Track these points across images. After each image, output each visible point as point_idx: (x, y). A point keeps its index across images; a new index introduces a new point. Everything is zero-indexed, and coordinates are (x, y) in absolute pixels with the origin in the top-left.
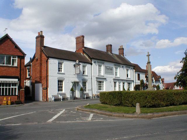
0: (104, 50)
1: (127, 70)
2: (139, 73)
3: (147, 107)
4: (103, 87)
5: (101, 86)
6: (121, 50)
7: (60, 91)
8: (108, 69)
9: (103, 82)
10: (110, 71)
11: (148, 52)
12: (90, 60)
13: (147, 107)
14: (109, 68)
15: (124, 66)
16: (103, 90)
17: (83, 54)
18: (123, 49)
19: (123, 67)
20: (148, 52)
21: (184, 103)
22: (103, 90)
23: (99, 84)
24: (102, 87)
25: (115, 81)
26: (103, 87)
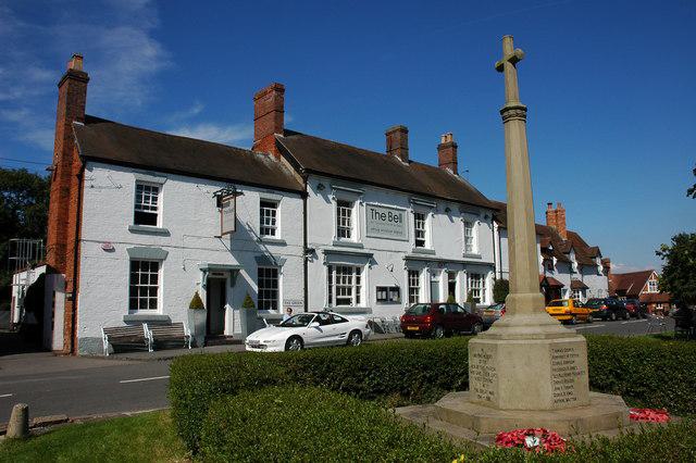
8: (382, 217)
14: (386, 211)
17: (278, 158)
24: (481, 292)
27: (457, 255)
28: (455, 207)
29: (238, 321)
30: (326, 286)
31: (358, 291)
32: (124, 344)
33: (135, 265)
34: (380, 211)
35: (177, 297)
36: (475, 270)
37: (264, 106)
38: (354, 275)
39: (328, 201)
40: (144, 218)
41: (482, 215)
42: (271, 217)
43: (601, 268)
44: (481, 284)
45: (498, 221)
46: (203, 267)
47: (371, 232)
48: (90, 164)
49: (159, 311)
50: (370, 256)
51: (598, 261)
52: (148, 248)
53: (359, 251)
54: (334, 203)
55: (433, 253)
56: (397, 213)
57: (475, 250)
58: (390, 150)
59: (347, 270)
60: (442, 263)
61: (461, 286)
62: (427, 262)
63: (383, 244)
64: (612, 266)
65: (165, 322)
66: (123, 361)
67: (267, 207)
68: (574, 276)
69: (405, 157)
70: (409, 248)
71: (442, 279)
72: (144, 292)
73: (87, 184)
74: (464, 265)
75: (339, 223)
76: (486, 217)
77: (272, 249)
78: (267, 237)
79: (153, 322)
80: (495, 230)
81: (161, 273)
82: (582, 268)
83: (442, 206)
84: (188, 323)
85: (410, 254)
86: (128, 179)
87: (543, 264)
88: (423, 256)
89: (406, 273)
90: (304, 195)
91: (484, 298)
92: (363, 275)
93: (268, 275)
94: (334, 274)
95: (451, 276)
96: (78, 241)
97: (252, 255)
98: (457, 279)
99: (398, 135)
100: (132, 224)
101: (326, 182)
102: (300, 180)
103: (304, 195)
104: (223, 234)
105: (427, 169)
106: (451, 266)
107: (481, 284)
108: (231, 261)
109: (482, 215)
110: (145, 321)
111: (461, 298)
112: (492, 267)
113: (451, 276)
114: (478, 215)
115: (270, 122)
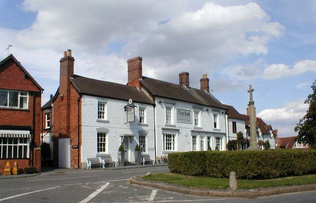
0: (176, 81)
1: (215, 116)
4: (174, 145)
5: (171, 143)
6: (205, 81)
7: (101, 151)
8: (182, 113)
14: (184, 111)
16: (174, 149)
17: (140, 89)
22: (174, 149)
24: (172, 144)
25: (195, 134)
26: (174, 145)
27: (211, 129)
28: (210, 109)
29: (133, 156)
30: (163, 143)
31: (174, 144)
32: (96, 166)
33: (99, 135)
34: (182, 111)
35: (112, 149)
36: (218, 136)
37: (133, 66)
38: (172, 138)
39: (163, 108)
40: (100, 114)
41: (221, 112)
42: (102, 107)
43: (272, 135)
44: (172, 140)
45: (227, 114)
46: (122, 135)
47: (179, 120)
48: (83, 96)
49: (107, 152)
50: (178, 130)
51: (271, 132)
52: (103, 128)
53: (201, 130)
54: (165, 108)
55: (220, 130)
56: (187, 112)
57: (199, 125)
58: (181, 83)
59: (170, 136)
60: (206, 133)
61: (213, 143)
62: (199, 132)
63: (183, 125)
64: (278, 133)
65: (109, 157)
66: (95, 171)
67: (142, 110)
68: (260, 139)
69: (188, 86)
70: (192, 127)
71: (205, 140)
72: (101, 144)
73: (82, 104)
74: (214, 133)
75: (99, 109)
76: (223, 113)
77: (144, 128)
78: (101, 119)
79: (103, 157)
80: (226, 118)
81: (107, 138)
82: (263, 134)
83: (205, 108)
84: (115, 159)
85: (193, 129)
86: (95, 101)
87: (247, 133)
88: (198, 130)
89: (192, 137)
90: (154, 106)
91: (174, 147)
92: (176, 138)
93: (142, 138)
94: (165, 137)
95: (209, 138)
96: (79, 126)
97: (137, 130)
98: (211, 140)
99: (185, 76)
100: (97, 119)
101: (162, 100)
102: (151, 99)
103: (154, 106)
104: (128, 122)
105: (197, 91)
106: (209, 134)
107: (172, 140)
108: (130, 133)
109: (221, 112)
110: (100, 156)
111: (213, 147)
112: (225, 134)
113: (209, 138)
114: (219, 112)
115: (136, 73)
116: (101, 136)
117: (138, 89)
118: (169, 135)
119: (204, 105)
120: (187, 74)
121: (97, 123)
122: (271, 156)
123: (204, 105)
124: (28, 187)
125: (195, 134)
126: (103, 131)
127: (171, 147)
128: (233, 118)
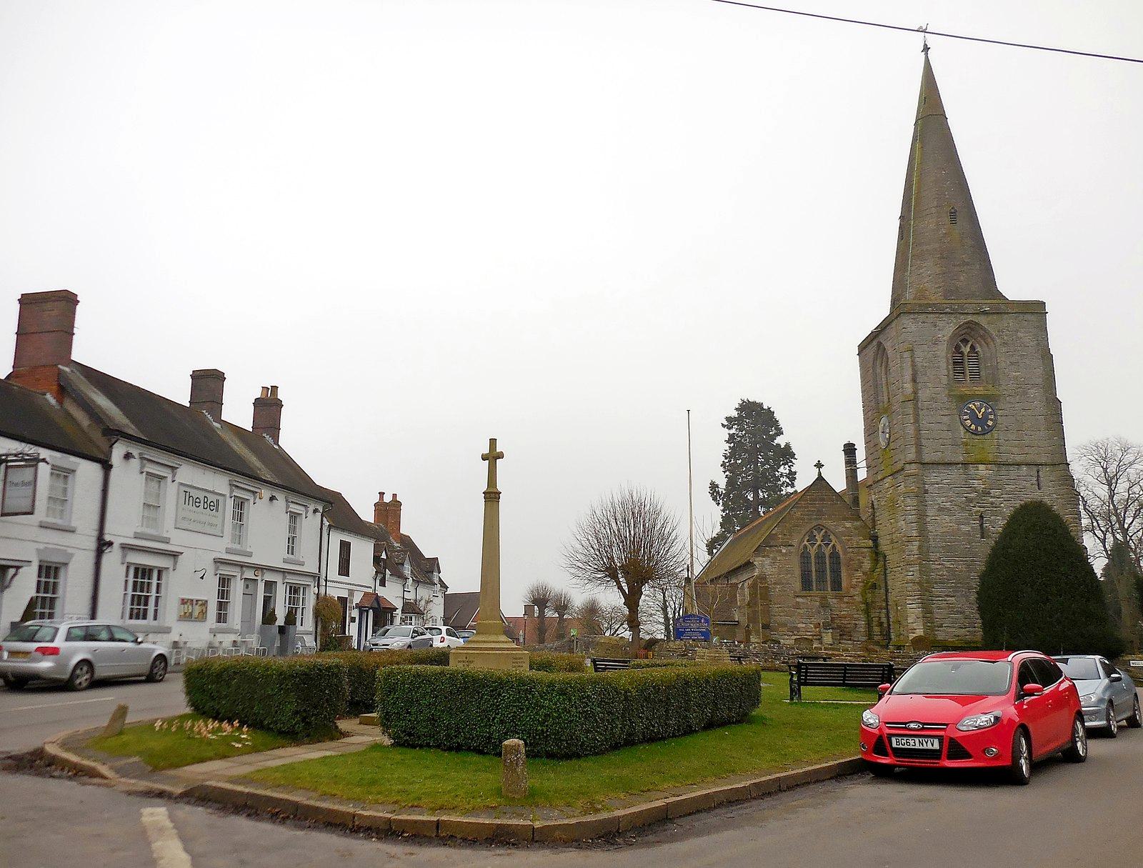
0: (180, 394)
1: (294, 517)
2: (347, 538)
3: (1120, 728)
4: (156, 604)
5: (147, 598)
6: (268, 406)
7: (138, 618)
8: (196, 502)
9: (160, 573)
10: (204, 515)
11: (493, 442)
12: (97, 435)
13: (1120, 728)
14: (201, 495)
15: (281, 496)
16: (155, 618)
17: (60, 402)
18: (279, 404)
19: (272, 498)
20: (493, 442)
21: (22, 683)
22: (155, 618)
23: (135, 583)
24: (152, 601)
25: (226, 571)
26: (156, 604)
34: (195, 493)
36: (293, 580)
38: (154, 581)
41: (311, 508)
69: (217, 416)
116: (48, 576)
117: (53, 401)
118: (144, 571)
119: (265, 481)
120: (67, 301)
121: (112, 540)
122: (246, 672)
123: (265, 481)
124: (110, 696)
125: (226, 571)
126: (55, 559)
127: (145, 611)
128: (343, 530)
